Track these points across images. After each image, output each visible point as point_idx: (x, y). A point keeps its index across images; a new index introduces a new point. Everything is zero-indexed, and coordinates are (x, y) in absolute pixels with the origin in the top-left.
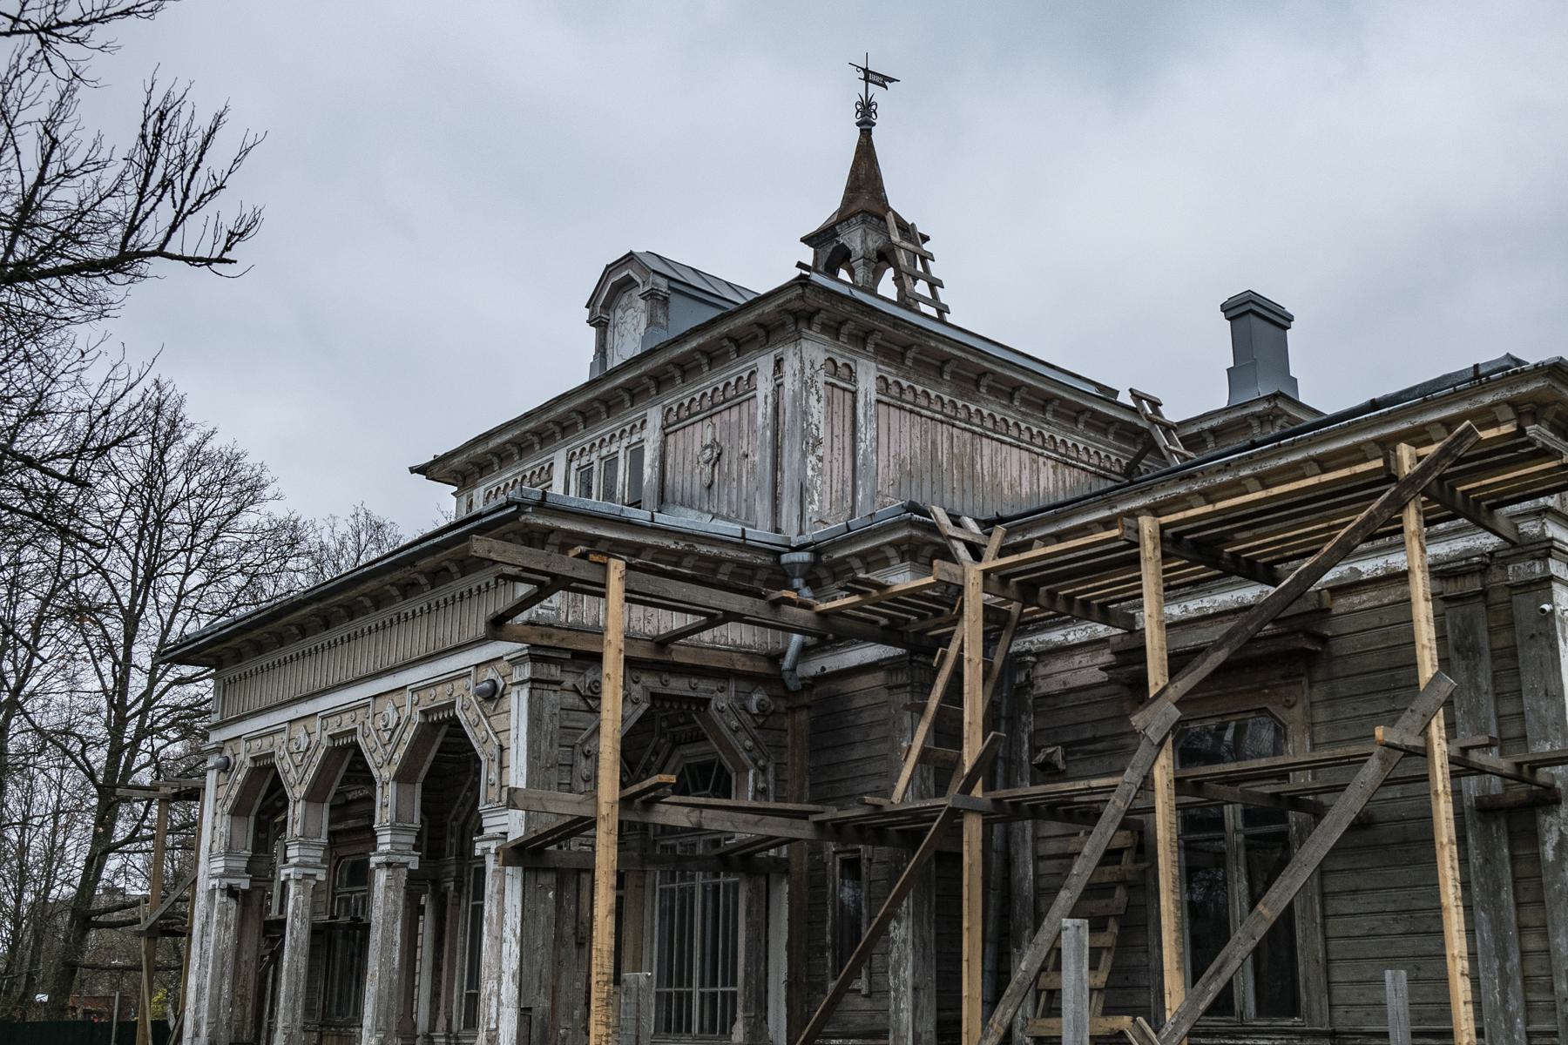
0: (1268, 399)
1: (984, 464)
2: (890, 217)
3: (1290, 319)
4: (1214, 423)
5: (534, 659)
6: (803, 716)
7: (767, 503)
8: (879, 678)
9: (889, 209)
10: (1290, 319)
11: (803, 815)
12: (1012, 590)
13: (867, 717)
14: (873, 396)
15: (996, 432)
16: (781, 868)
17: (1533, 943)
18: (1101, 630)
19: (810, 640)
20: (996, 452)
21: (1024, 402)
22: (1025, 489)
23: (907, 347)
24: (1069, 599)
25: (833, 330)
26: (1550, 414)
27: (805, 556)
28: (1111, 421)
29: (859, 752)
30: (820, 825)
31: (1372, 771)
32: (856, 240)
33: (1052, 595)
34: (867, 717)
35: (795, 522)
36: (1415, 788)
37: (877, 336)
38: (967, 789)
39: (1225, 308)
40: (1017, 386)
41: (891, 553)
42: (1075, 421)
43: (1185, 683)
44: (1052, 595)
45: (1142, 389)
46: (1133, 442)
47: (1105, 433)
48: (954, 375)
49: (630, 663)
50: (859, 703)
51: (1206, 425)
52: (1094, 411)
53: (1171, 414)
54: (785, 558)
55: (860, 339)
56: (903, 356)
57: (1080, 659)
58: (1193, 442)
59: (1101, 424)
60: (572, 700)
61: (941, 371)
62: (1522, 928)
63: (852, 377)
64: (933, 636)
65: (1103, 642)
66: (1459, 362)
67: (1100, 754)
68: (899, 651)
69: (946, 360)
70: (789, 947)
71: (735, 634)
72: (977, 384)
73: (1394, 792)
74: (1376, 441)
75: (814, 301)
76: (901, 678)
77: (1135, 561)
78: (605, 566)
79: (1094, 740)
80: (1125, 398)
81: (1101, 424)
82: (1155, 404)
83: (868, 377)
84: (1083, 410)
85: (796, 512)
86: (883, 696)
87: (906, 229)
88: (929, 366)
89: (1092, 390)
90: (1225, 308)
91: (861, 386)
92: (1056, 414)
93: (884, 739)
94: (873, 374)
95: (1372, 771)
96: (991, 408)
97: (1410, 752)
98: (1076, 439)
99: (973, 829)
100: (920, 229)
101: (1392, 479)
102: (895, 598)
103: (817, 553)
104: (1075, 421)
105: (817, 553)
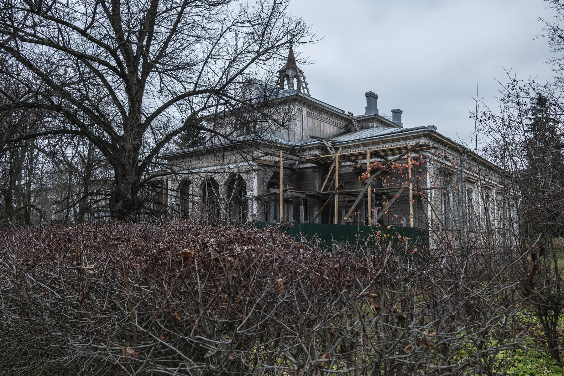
0: (374, 115)
1: (322, 127)
2: (297, 69)
3: (378, 97)
4: (363, 119)
5: (258, 165)
6: (296, 175)
7: (287, 135)
8: (312, 169)
9: (297, 67)
10: (378, 97)
11: (304, 193)
12: (342, 158)
13: (309, 176)
14: (305, 115)
15: (324, 120)
16: (292, 202)
17: (420, 215)
18: (352, 163)
19: (300, 162)
20: (324, 124)
21: (329, 114)
22: (329, 132)
23: (311, 105)
24: (349, 159)
25: (300, 102)
26: (429, 136)
27: (299, 147)
28: (344, 117)
29: (307, 182)
30: (306, 195)
31: (401, 190)
32: (290, 73)
33: (347, 158)
34: (309, 176)
35: (293, 140)
36: (407, 192)
37: (307, 104)
38: (336, 190)
39: (366, 94)
40: (328, 112)
41: (315, 148)
42: (337, 118)
43: (374, 176)
44: (347, 158)
45: (350, 111)
46: (347, 121)
47: (342, 120)
48: (318, 110)
49: (284, 168)
50: (307, 174)
51: (361, 119)
52: (341, 116)
53: (355, 115)
54: (295, 148)
55: (304, 104)
56: (310, 107)
57: (347, 168)
58: (359, 122)
59: (342, 118)
60: (263, 173)
61: (316, 109)
62: (418, 213)
63: (302, 111)
64: (129, 114)
65: (352, 165)
66: (416, 126)
67: (351, 184)
68: (316, 165)
69: (317, 107)
70: (293, 216)
71: (269, 158)
72: (322, 111)
73: (405, 192)
74: (402, 138)
75: (298, 97)
76: (316, 170)
77: (366, 154)
78: (280, 152)
79: (350, 182)
80: (346, 113)
81: (342, 118)
82: (352, 114)
83: (305, 110)
84: (339, 116)
85: (293, 138)
86: (312, 173)
87: (300, 71)
88: (314, 108)
89: (341, 112)
90: (366, 94)
91: (304, 113)
92: (334, 116)
93: (313, 180)
94: (305, 110)
95: (401, 190)
96: (324, 116)
97: (407, 188)
98: (337, 121)
99: (336, 197)
100: (303, 71)
101: (407, 149)
102: (321, 158)
103: (301, 147)
104: (337, 118)
105: (301, 147)
